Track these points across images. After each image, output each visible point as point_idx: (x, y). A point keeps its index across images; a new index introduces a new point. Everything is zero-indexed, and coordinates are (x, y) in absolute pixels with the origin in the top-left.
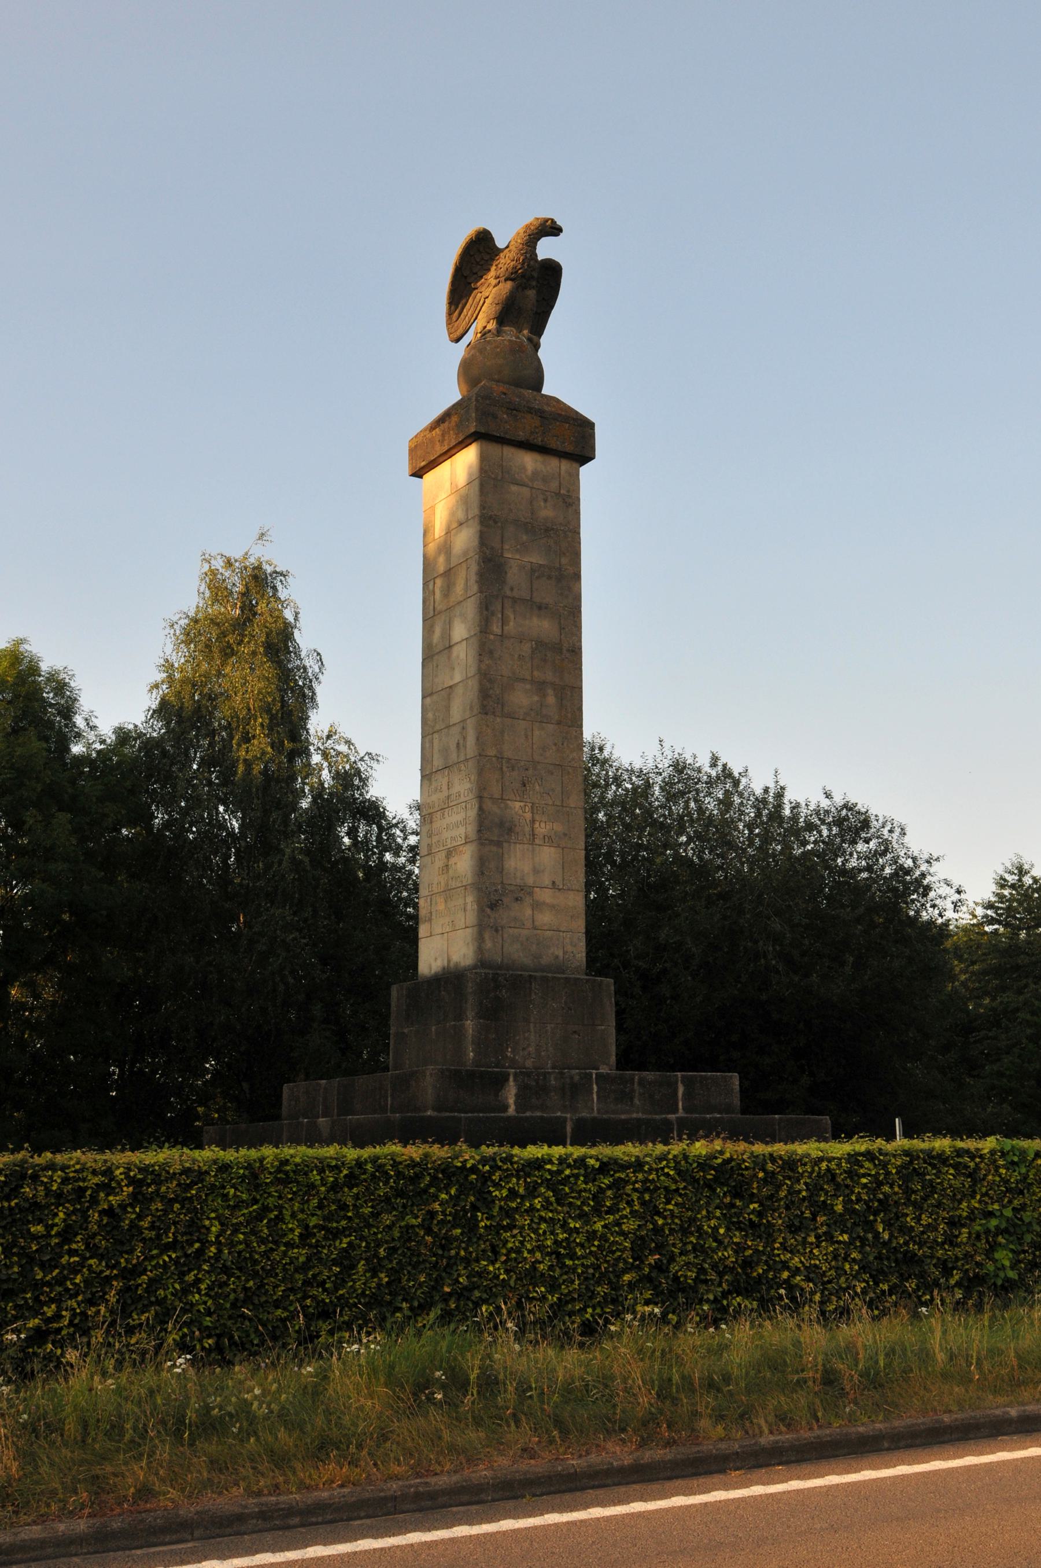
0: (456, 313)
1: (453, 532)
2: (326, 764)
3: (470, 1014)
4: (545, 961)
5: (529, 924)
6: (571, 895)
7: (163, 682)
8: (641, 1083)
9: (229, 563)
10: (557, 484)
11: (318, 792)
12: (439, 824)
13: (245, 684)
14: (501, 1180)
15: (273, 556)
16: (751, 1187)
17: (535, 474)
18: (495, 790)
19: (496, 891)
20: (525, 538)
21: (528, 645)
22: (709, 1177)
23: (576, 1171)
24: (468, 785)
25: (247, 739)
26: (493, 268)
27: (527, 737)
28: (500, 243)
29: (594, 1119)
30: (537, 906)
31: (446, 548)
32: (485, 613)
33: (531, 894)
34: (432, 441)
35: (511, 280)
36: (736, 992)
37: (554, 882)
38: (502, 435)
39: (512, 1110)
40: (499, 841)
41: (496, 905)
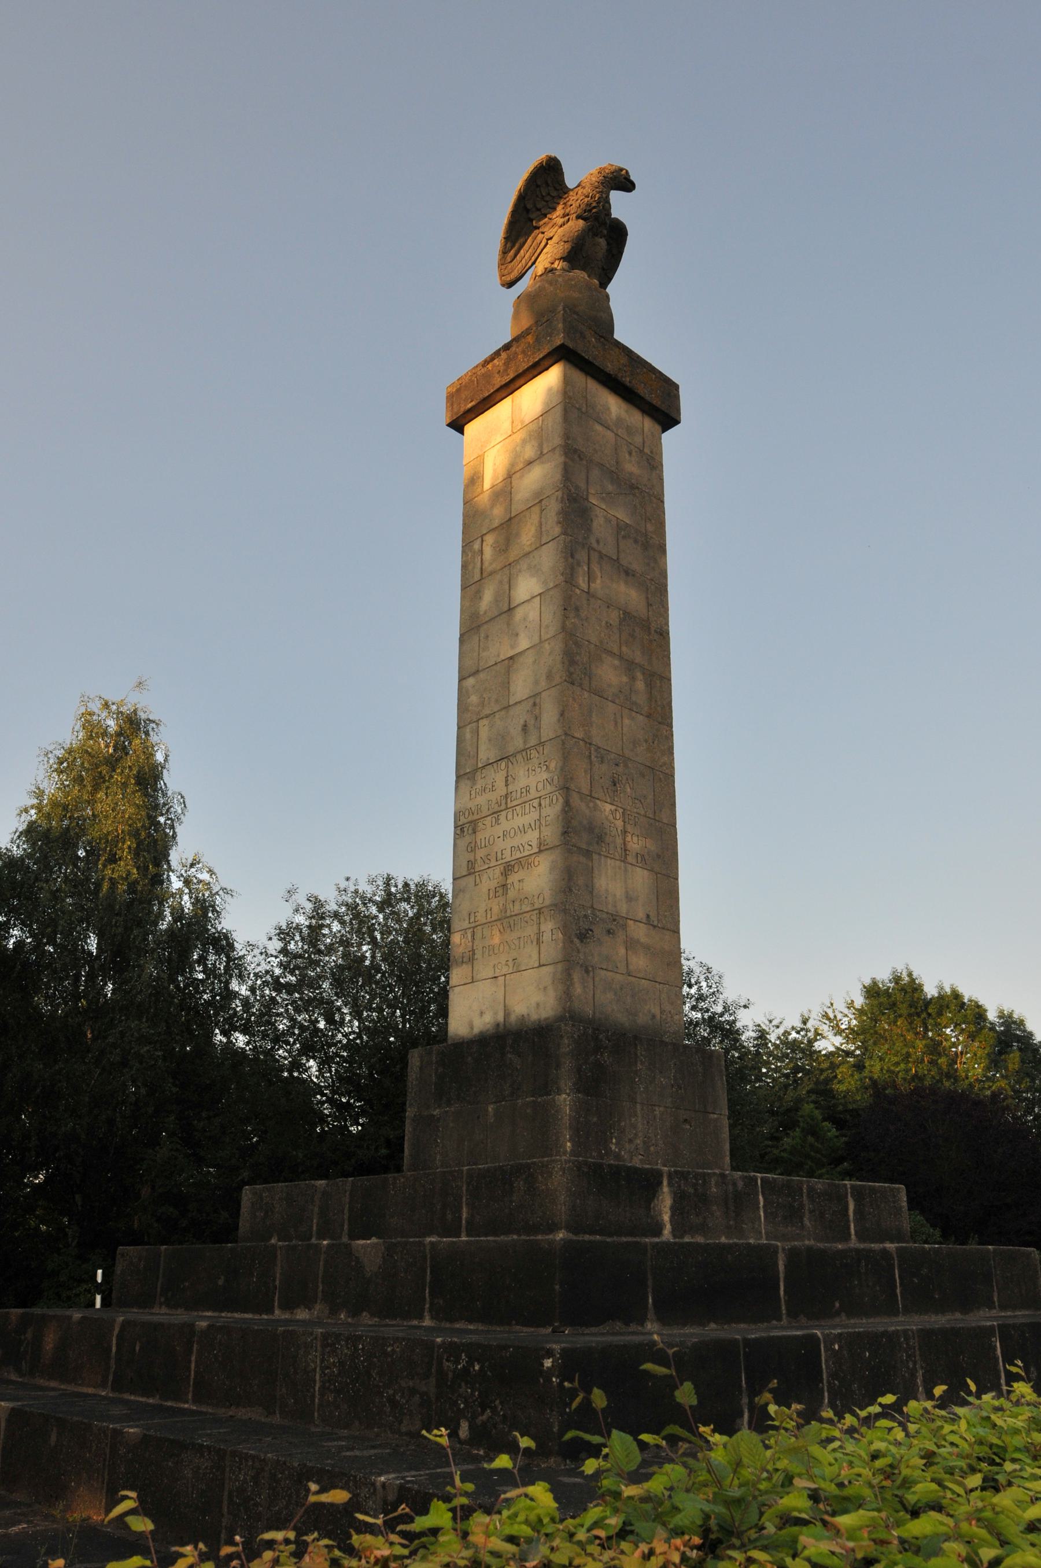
0: (512, 253)
3: (566, 1083)
4: (642, 1019)
5: (622, 969)
7: (32, 807)
9: (106, 705)
11: (178, 914)
15: (149, 705)
18: (583, 783)
19: (586, 916)
20: (610, 488)
25: (113, 859)
26: (560, 208)
27: (616, 724)
28: (570, 181)
30: (631, 944)
31: (505, 491)
32: (570, 559)
33: (624, 927)
34: (488, 376)
38: (591, 359)
40: (588, 851)
41: (585, 937)
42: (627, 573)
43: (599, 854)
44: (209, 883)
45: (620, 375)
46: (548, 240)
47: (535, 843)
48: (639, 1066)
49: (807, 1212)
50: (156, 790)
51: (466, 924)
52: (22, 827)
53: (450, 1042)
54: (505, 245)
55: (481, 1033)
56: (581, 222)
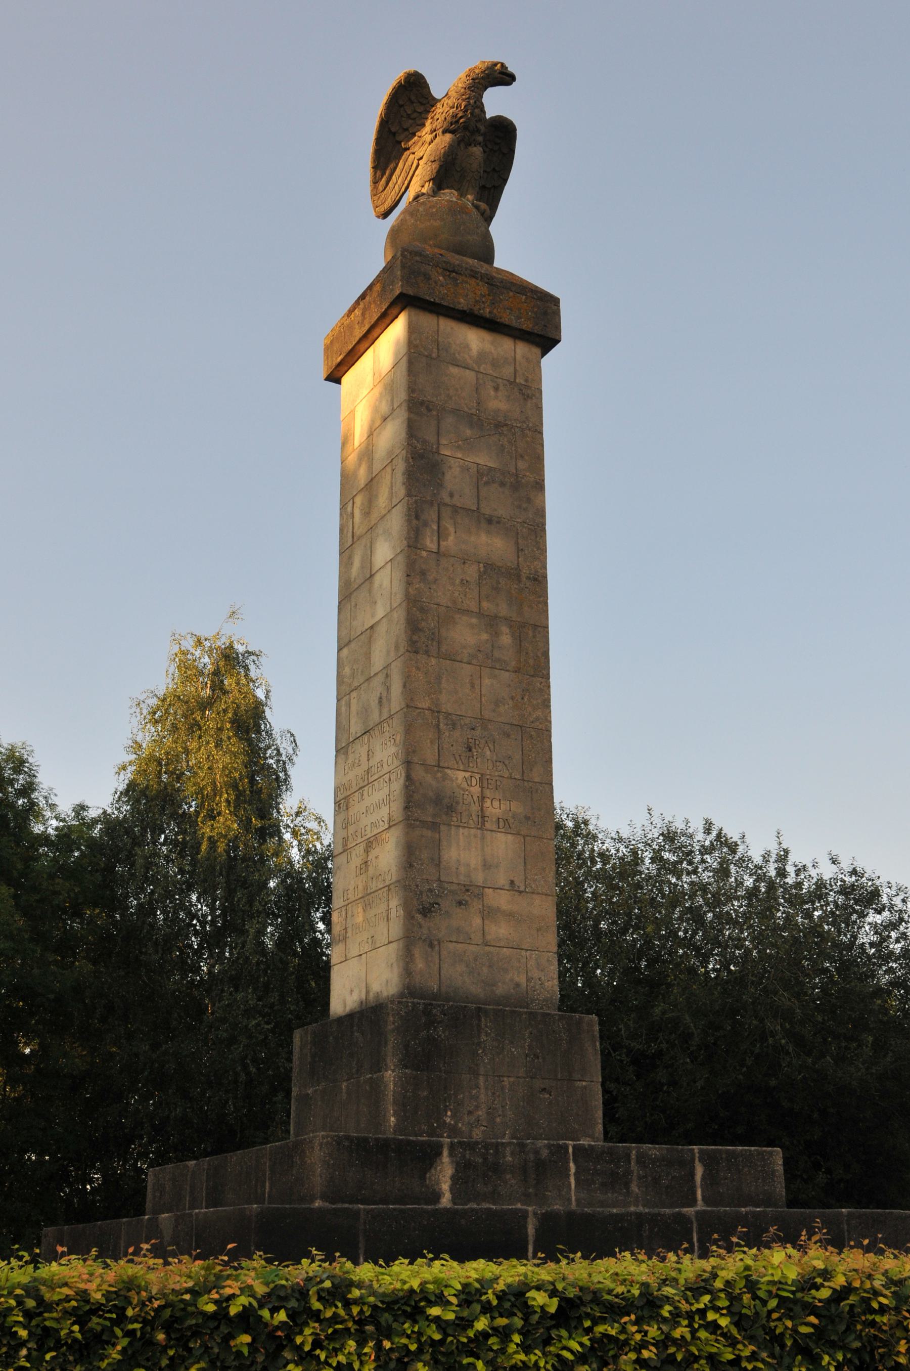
1: (375, 434)
2: (295, 843)
3: (391, 1061)
4: (500, 990)
5: (477, 938)
6: (537, 900)
7: (131, 763)
8: (642, 1160)
9: (199, 642)
10: (512, 369)
11: (289, 873)
12: (357, 808)
13: (212, 761)
14: (317, 1344)
16: (892, 1352)
17: (482, 356)
19: (430, 890)
20: (468, 432)
21: (474, 568)
22: (804, 1330)
23: (502, 1322)
24: (393, 750)
27: (473, 686)
28: (437, 91)
29: (570, 1214)
30: (489, 913)
31: (367, 453)
32: (414, 522)
33: (480, 896)
34: (350, 327)
35: (450, 132)
36: (741, 1077)
37: (512, 882)
38: (437, 301)
39: (446, 1201)
41: (430, 911)
42: (490, 521)
43: (449, 825)
44: (317, 833)
45: (476, 308)
46: (419, 160)
47: (386, 819)
48: (483, 1038)
49: (635, 1178)
50: (259, 731)
51: (342, 903)
52: (122, 787)
53: (331, 1018)
54: (375, 173)
55: (351, 1010)
56: (448, 137)
